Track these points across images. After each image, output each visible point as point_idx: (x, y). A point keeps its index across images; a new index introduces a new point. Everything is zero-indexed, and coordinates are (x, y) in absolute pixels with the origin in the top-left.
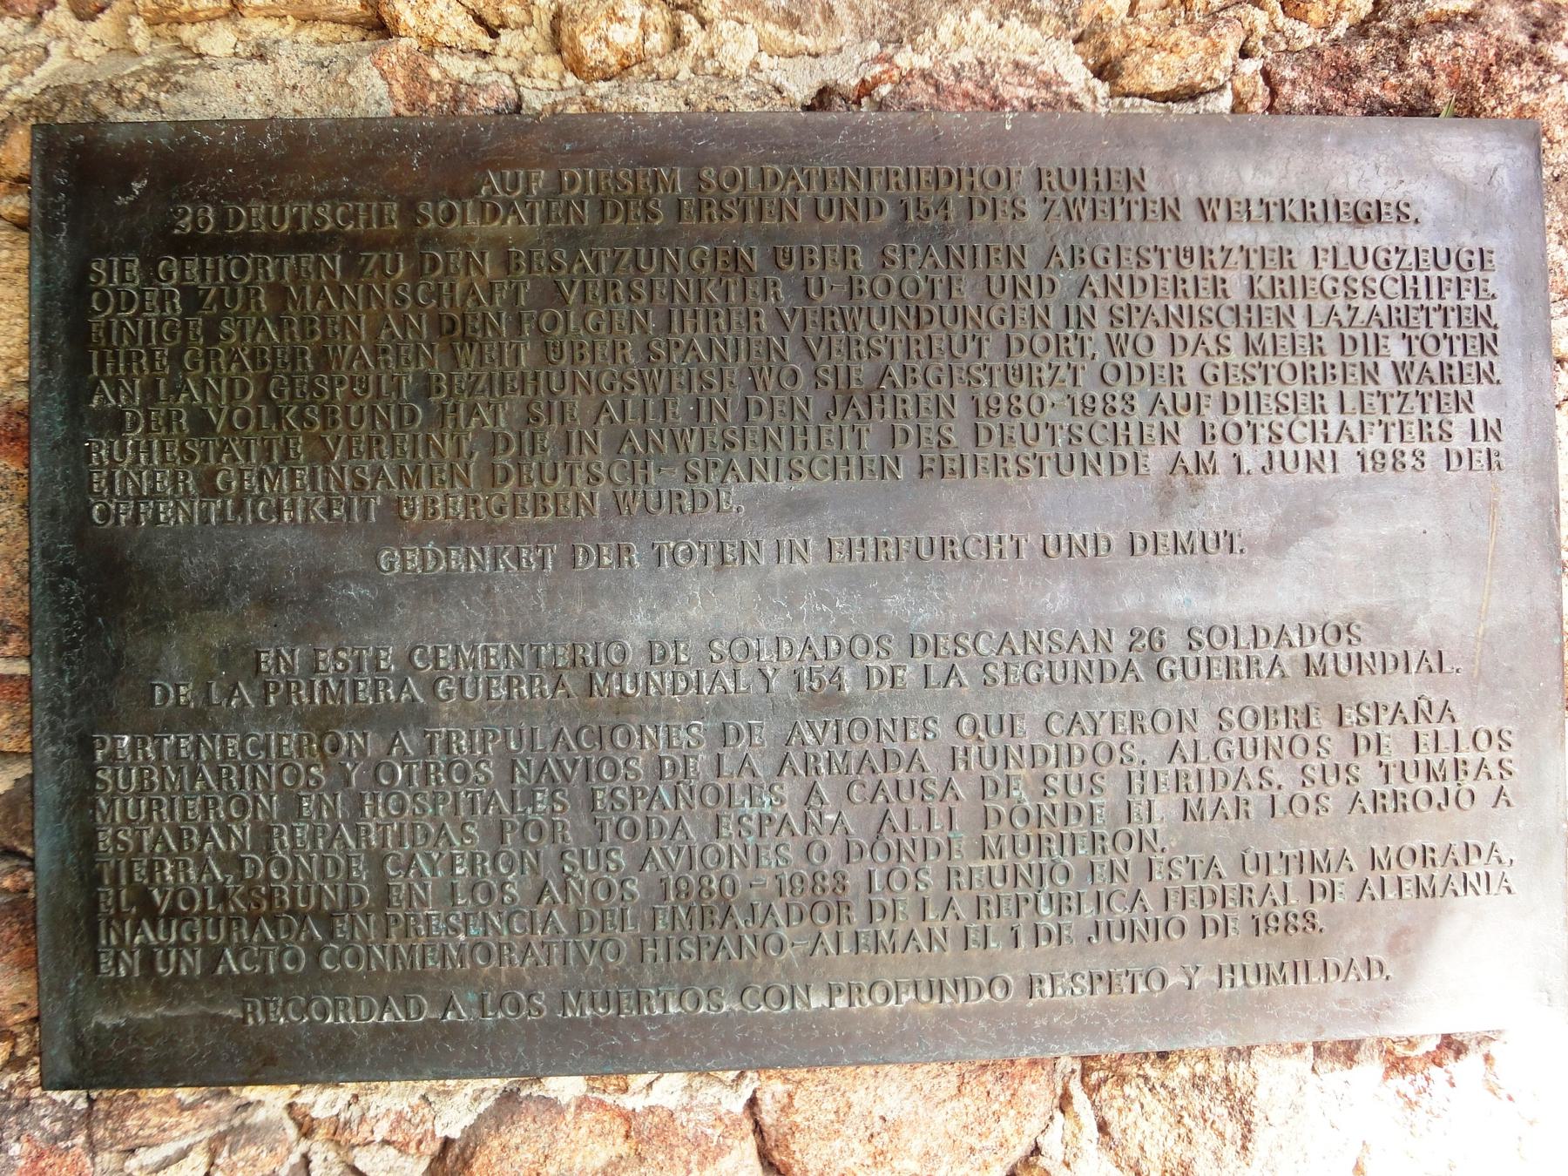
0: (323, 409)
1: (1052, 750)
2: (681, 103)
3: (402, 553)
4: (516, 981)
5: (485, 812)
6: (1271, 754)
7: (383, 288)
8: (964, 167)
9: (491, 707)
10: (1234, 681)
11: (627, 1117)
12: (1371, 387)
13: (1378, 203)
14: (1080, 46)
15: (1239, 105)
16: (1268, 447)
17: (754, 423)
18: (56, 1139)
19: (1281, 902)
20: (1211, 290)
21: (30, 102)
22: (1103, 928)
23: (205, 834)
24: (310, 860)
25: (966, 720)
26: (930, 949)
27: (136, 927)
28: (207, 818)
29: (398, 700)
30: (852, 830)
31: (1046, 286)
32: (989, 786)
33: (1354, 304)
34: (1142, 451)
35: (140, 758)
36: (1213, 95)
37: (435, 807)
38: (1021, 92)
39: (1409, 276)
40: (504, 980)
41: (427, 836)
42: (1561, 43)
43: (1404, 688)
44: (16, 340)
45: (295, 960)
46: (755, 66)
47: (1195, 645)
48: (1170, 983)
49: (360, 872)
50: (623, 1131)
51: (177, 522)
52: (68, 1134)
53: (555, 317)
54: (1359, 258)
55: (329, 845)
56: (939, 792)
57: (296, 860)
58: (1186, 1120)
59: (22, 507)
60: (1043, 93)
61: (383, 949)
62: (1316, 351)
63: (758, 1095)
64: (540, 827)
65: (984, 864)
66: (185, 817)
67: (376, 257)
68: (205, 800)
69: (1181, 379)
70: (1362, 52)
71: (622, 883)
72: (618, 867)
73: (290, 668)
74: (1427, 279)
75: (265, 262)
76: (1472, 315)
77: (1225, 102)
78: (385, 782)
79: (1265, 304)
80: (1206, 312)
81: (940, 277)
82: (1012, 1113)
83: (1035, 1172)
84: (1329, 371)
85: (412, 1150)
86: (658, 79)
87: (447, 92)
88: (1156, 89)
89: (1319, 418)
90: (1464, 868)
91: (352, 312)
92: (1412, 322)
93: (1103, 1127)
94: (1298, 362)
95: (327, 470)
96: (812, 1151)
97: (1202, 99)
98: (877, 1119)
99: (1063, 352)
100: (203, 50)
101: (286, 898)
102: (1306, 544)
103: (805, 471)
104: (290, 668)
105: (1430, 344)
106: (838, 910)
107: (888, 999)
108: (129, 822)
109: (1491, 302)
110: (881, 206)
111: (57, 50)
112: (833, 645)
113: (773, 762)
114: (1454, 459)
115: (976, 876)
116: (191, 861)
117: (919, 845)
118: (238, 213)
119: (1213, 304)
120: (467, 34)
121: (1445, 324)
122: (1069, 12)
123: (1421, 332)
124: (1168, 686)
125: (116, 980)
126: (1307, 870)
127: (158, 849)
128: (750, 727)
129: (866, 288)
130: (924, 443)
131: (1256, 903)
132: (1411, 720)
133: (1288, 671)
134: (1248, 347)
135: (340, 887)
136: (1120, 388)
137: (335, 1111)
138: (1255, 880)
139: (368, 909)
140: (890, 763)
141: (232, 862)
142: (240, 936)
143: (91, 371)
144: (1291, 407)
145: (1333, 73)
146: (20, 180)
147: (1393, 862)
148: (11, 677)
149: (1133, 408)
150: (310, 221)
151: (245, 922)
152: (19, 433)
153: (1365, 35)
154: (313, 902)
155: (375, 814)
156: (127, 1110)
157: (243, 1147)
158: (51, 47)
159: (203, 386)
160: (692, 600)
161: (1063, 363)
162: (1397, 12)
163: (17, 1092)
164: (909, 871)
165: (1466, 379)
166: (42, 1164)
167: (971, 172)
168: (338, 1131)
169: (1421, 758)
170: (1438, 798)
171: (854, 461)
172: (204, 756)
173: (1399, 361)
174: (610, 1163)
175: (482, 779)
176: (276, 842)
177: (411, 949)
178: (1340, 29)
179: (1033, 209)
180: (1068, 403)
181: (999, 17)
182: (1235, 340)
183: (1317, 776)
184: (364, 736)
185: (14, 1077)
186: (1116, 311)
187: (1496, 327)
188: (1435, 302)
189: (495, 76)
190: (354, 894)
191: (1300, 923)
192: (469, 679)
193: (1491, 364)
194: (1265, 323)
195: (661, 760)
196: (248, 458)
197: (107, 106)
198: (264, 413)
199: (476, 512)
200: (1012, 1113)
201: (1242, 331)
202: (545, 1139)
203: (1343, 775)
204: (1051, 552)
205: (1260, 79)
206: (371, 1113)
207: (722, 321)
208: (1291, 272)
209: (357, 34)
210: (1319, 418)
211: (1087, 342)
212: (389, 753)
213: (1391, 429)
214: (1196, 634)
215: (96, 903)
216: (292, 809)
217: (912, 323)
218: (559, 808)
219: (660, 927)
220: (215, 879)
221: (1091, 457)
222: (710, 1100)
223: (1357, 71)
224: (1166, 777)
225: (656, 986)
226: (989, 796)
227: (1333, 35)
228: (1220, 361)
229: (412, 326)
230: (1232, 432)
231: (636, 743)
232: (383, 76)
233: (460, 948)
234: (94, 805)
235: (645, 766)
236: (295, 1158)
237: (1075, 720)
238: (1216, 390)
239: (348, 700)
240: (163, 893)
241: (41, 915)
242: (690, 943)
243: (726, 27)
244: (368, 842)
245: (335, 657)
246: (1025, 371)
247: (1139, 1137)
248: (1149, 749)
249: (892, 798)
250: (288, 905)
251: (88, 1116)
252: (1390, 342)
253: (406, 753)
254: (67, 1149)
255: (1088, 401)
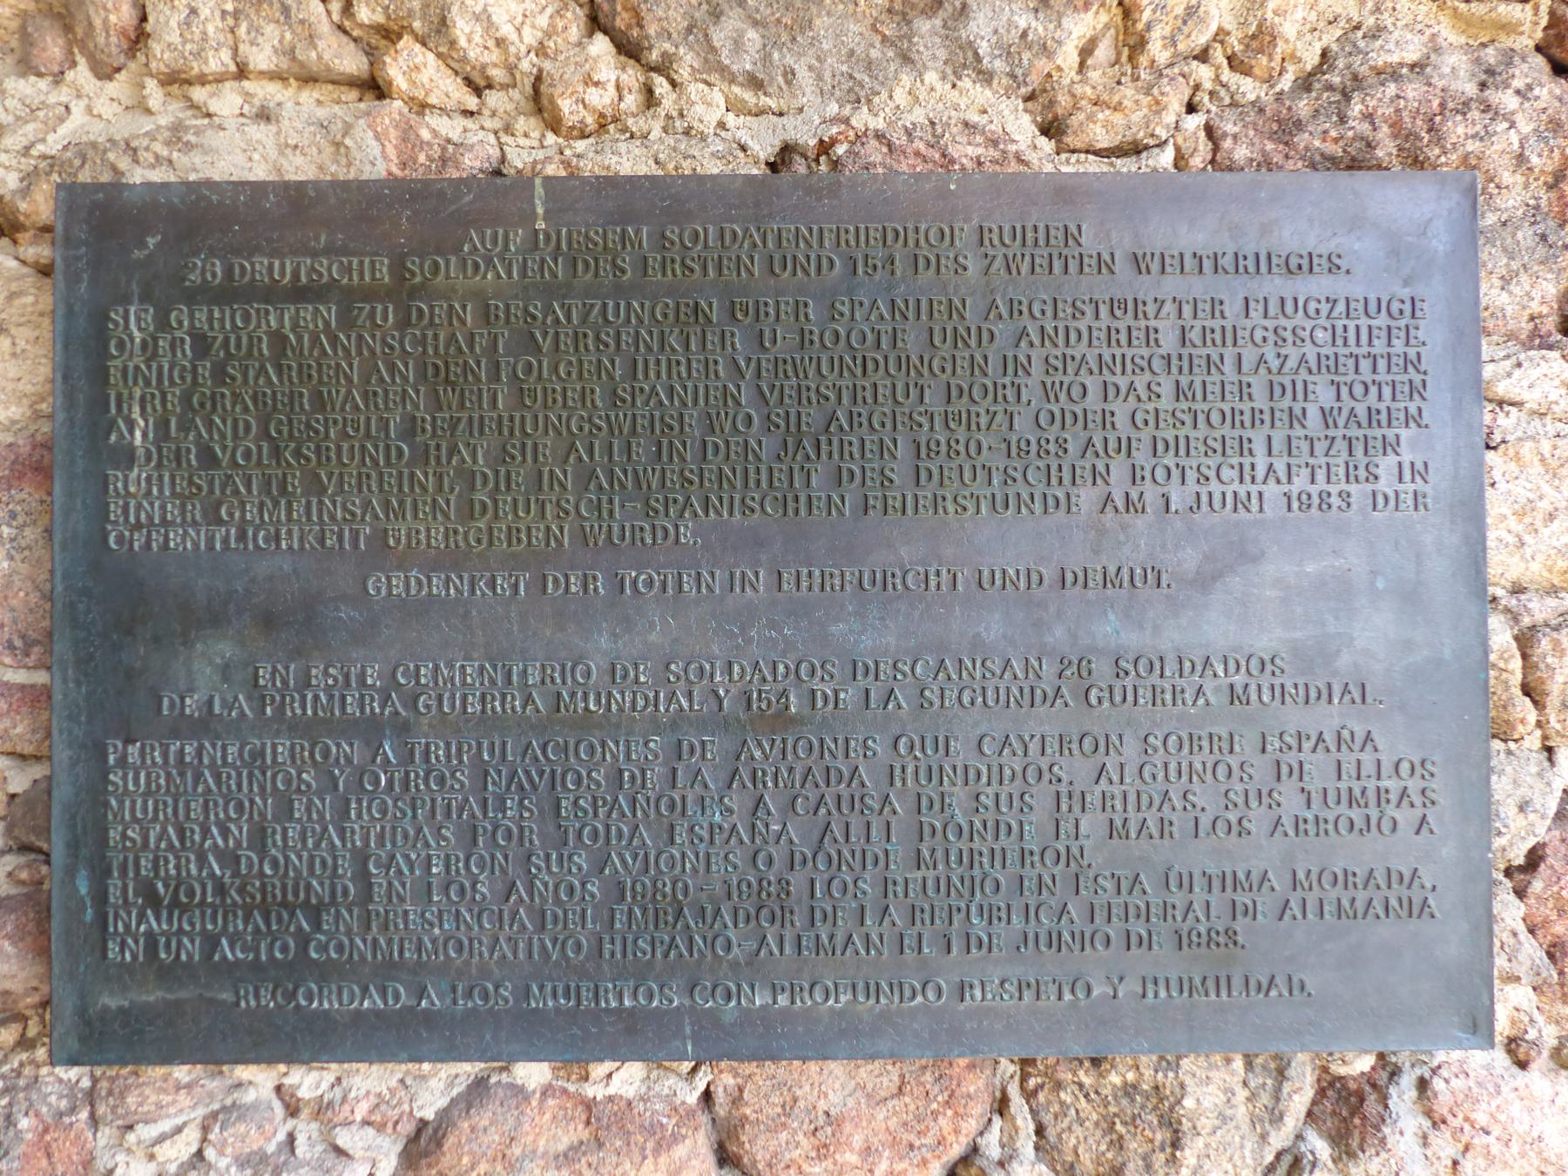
0: (318, 448)
1: (984, 770)
2: (651, 162)
3: (389, 579)
4: (485, 972)
5: (460, 817)
6: (1195, 778)
7: (373, 337)
8: (910, 226)
9: (467, 721)
10: (1159, 707)
11: (589, 1105)
12: (1298, 431)
13: (1310, 254)
14: (1029, 104)
15: (1180, 161)
16: (1197, 488)
17: (711, 462)
18: (61, 1115)
19: (1203, 919)
20: (1144, 340)
21: (52, 157)
22: (1031, 936)
23: (206, 832)
24: (300, 858)
25: (904, 740)
26: (868, 952)
27: (142, 917)
28: (207, 818)
29: (382, 714)
30: (796, 840)
31: (985, 336)
32: (924, 802)
33: (1283, 352)
34: (1074, 491)
35: (149, 762)
36: (1156, 150)
37: (414, 810)
38: (970, 150)
39: (1339, 324)
40: (474, 971)
41: (406, 836)
42: (1510, 91)
43: (1328, 718)
44: (41, 379)
45: (284, 949)
46: (722, 125)
47: (1122, 674)
48: (1095, 993)
49: (346, 868)
50: (584, 1117)
51: (185, 548)
52: (73, 1110)
53: (530, 364)
54: (1289, 308)
55: (317, 845)
56: (877, 807)
57: (287, 858)
58: (1119, 1127)
59: (46, 531)
60: (991, 152)
61: (364, 941)
62: (1245, 397)
63: (712, 1088)
64: (509, 831)
65: (919, 875)
66: (188, 817)
67: (368, 307)
68: (206, 803)
69: (1113, 424)
70: (1303, 107)
71: (583, 884)
72: (580, 869)
73: (285, 682)
74: (1357, 327)
75: (267, 312)
76: (1401, 362)
77: (1166, 158)
78: (370, 788)
79: (1194, 352)
80: (1137, 360)
81: (886, 328)
82: (949, 1113)
83: (973, 1171)
84: (1257, 415)
85: (389, 1129)
86: (632, 137)
87: (436, 152)
88: (1099, 146)
89: (1247, 461)
90: (1385, 892)
91: (344, 358)
92: (1341, 369)
93: (1040, 1131)
94: (1227, 408)
95: (321, 503)
96: (761, 1143)
97: (1144, 155)
98: (820, 1113)
99: (1000, 399)
100: (212, 110)
101: (278, 892)
102: (1234, 581)
103: (757, 506)
104: (285, 682)
105: (1358, 390)
106: (780, 917)
107: (827, 999)
108: (135, 819)
109: (1422, 350)
110: (831, 262)
111: (78, 109)
112: (781, 668)
113: (724, 776)
114: (1380, 500)
115: (911, 886)
116: (193, 857)
117: (858, 855)
118: (243, 267)
119: (1145, 352)
120: (456, 95)
121: (1374, 371)
122: (1019, 72)
123: (1348, 379)
124: (1096, 712)
125: (123, 963)
126: (1229, 889)
127: (163, 845)
128: (703, 743)
129: (816, 339)
130: (868, 483)
131: (1179, 919)
132: (1333, 749)
133: (1212, 700)
134: (1178, 392)
135: (327, 882)
136: (1053, 432)
137: (319, 1092)
138: (1178, 898)
139: (352, 903)
140: (833, 780)
141: (230, 858)
142: (236, 926)
143: (108, 411)
144: (1220, 450)
145: (1275, 127)
146: (47, 229)
147: (1315, 884)
148: (32, 686)
149: (1066, 451)
150: (308, 274)
151: (240, 913)
152: (36, 465)
153: (1308, 89)
154: (302, 895)
155: (359, 816)
156: (127, 1088)
157: (234, 1124)
158: (72, 106)
159: (210, 424)
160: (652, 625)
161: (1000, 408)
162: (1341, 66)
163: (27, 1071)
164: (849, 880)
165: (1395, 423)
166: (48, 1138)
167: (917, 230)
168: (322, 1109)
169: (1343, 785)
170: (1359, 823)
171: (803, 499)
172: (206, 761)
173: (1327, 407)
174: (571, 1148)
175: (457, 786)
176: (270, 841)
177: (390, 942)
178: (1286, 84)
179: (973, 266)
180: (1004, 446)
181: (952, 77)
182: (1166, 388)
183: (1240, 801)
184: (351, 745)
185: (24, 1056)
186: (1052, 360)
187: (1425, 373)
188: (1364, 350)
189: (481, 134)
190: (339, 889)
191: (1221, 940)
192: (447, 695)
193: (1420, 410)
194: (1196, 370)
195: (621, 772)
196: (249, 491)
197: (124, 164)
198: (265, 451)
199: (456, 542)
200: (949, 1113)
201: (1173, 378)
202: (511, 1121)
203: (1265, 800)
204: (986, 586)
205: (1202, 134)
206: (353, 1094)
207: (683, 369)
208: (1224, 323)
209: (354, 94)
210: (1247, 461)
211: (1023, 389)
212: (374, 761)
213: (1318, 471)
214: (1123, 663)
215: (106, 893)
216: (285, 811)
217: (859, 371)
218: (526, 815)
219: (618, 925)
220: (214, 874)
221: (1025, 496)
222: (666, 1091)
223: (1299, 125)
224: (1094, 798)
225: (613, 980)
226: (924, 811)
227: (1278, 89)
228: (1150, 407)
229: (400, 372)
230: (1160, 474)
231: (598, 755)
232: (377, 137)
233: (434, 941)
234: (107, 804)
235: (607, 777)
236: (281, 1136)
237: (1006, 741)
238: (1146, 434)
239: (337, 713)
240: (166, 886)
241: (54, 904)
242: (645, 941)
243: (695, 89)
244: (353, 842)
245: (326, 673)
246: (964, 416)
247: (1073, 1141)
248: (1076, 769)
249: (834, 812)
250: (279, 898)
251: (91, 1096)
252: (1318, 389)
253: (389, 761)
254: (71, 1124)
255: (1023, 445)
